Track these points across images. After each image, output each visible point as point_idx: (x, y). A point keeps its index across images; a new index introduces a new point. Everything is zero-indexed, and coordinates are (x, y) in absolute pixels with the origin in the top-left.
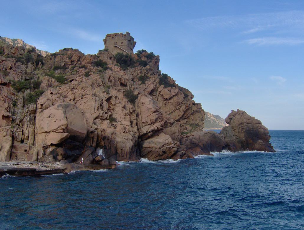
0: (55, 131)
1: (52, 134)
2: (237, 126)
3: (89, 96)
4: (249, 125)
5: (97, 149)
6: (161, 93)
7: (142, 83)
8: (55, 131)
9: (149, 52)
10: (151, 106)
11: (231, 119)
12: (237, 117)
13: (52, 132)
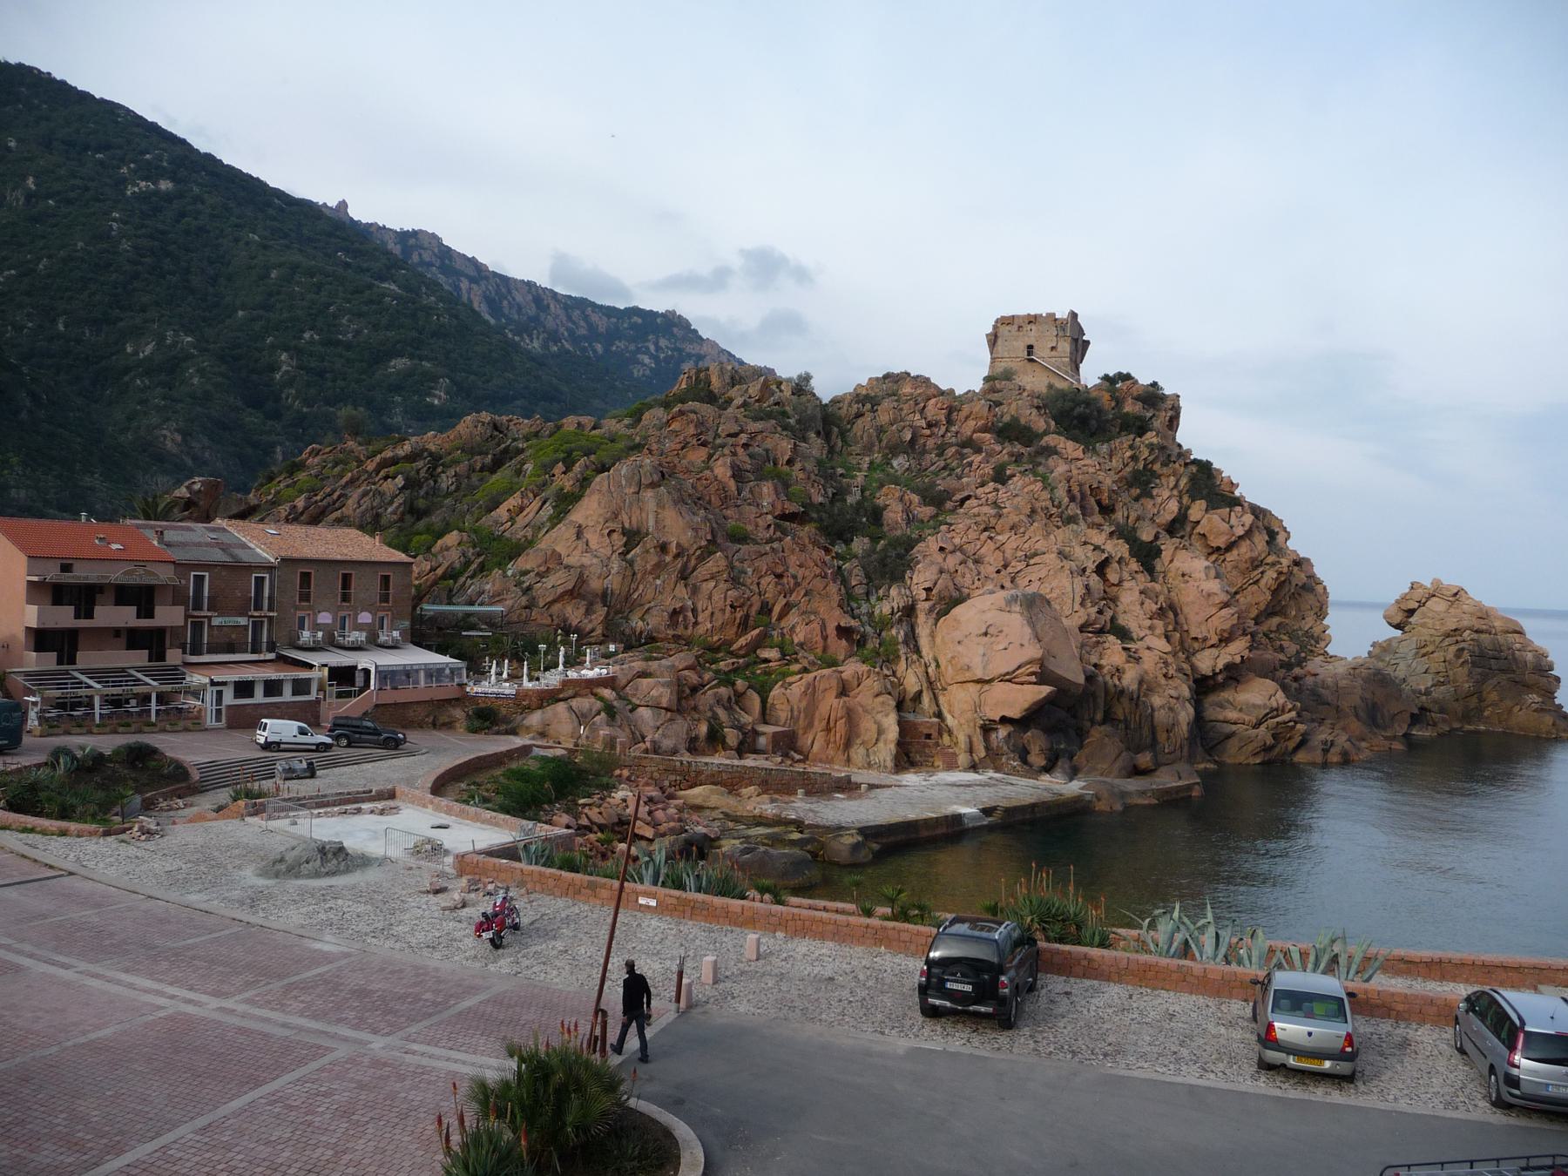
0: (1008, 678)
1: (999, 689)
2: (1438, 639)
3: (1051, 558)
4: (1483, 636)
5: (675, 697)
6: (1199, 529)
7: (675, 325)
8: (1008, 678)
9: (1144, 379)
10: (1214, 586)
11: (1411, 612)
12: (1436, 605)
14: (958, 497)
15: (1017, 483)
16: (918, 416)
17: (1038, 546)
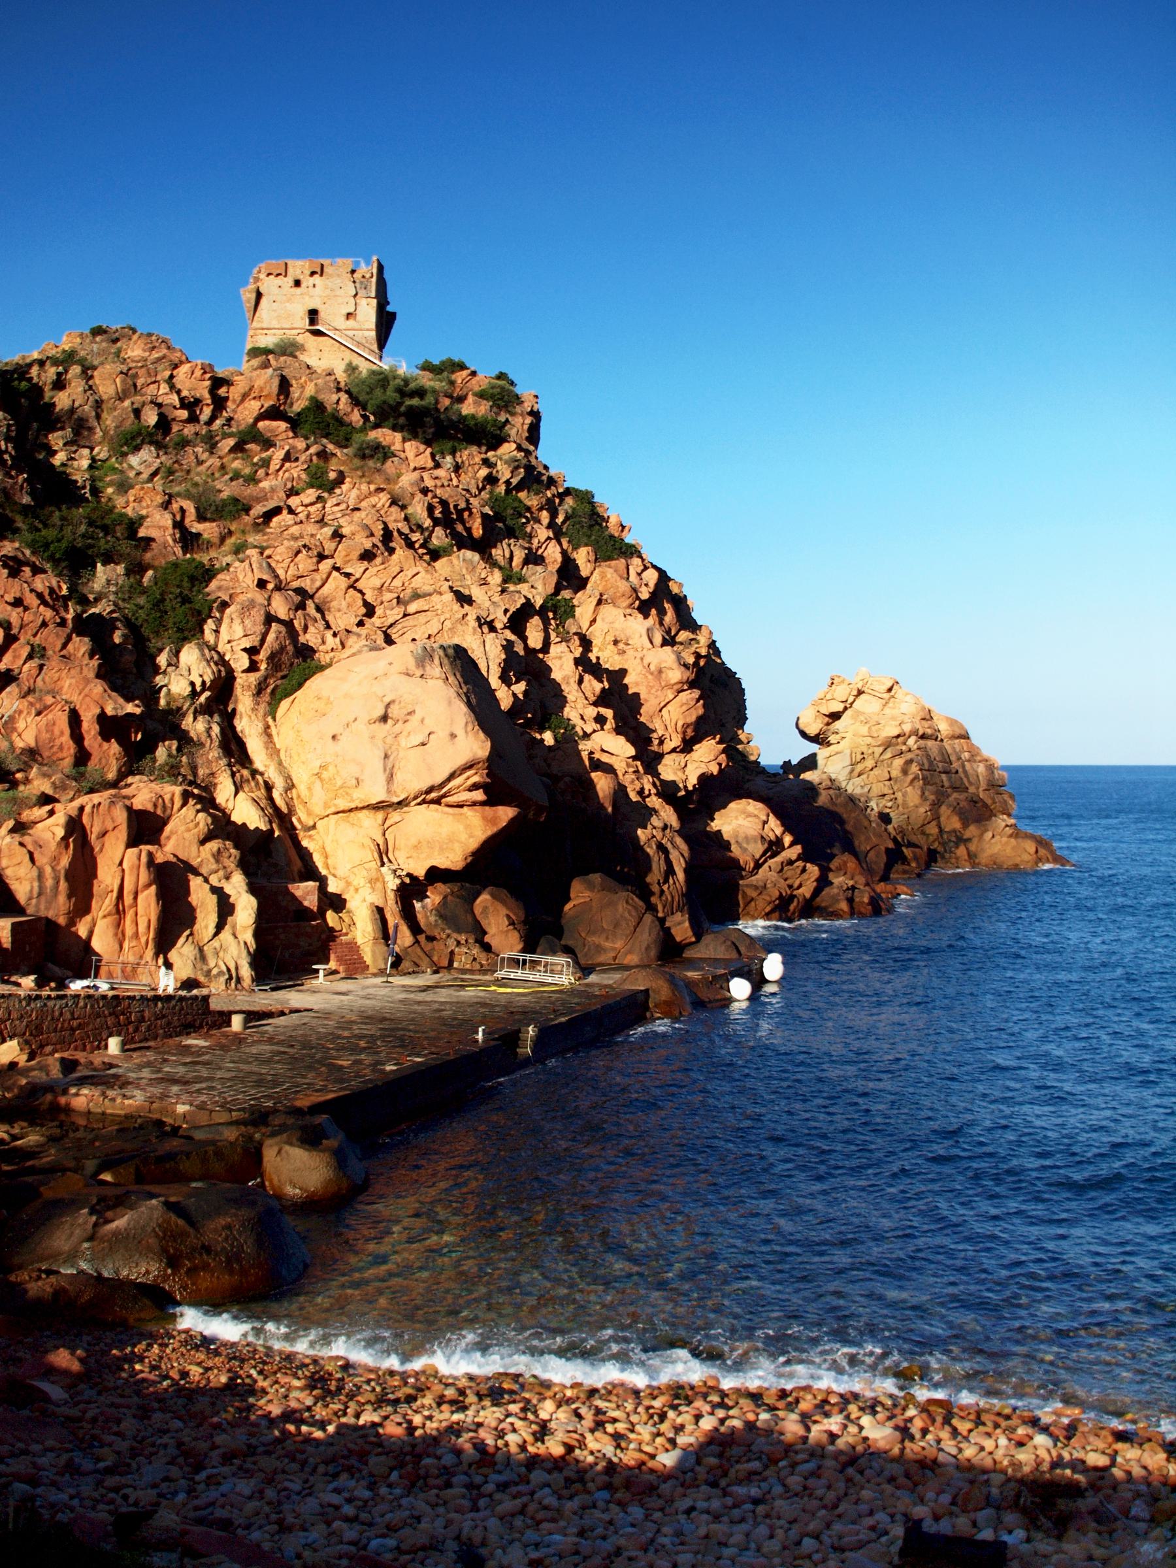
0: (433, 796)
8: (433, 796)
11: (835, 716)
13: (424, 802)
14: (258, 510)
15: (350, 491)
16: (164, 388)
17: (417, 583)
